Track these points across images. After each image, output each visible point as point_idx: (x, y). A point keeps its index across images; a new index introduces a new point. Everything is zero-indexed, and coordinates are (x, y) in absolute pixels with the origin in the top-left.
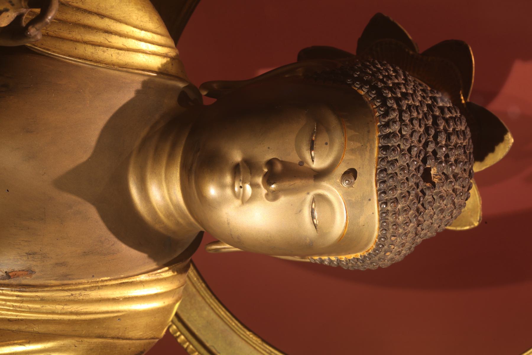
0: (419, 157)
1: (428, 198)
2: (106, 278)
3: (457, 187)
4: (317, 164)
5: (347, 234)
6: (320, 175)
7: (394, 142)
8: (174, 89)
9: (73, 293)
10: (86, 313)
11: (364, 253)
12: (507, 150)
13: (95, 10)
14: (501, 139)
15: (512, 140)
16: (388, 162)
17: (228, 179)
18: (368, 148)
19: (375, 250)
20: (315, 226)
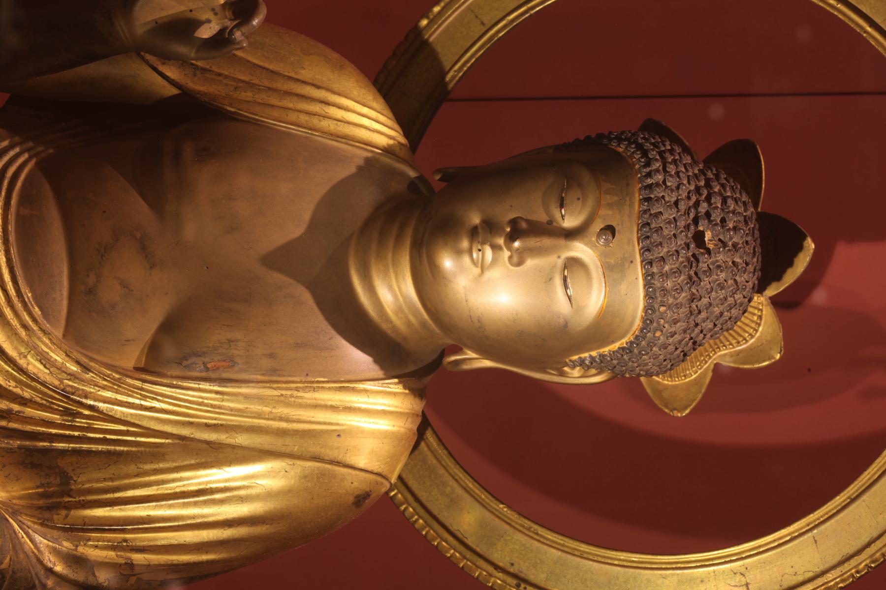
0: (689, 214)
1: (703, 266)
2: (322, 379)
3: (737, 260)
4: (570, 222)
5: (608, 306)
6: (571, 234)
7: (659, 192)
8: (403, 175)
9: (284, 392)
10: (299, 421)
11: (629, 338)
12: (808, 259)
13: (310, 81)
14: (800, 248)
15: (813, 246)
16: (651, 215)
17: (465, 244)
18: (628, 202)
19: (642, 330)
20: (569, 298)
